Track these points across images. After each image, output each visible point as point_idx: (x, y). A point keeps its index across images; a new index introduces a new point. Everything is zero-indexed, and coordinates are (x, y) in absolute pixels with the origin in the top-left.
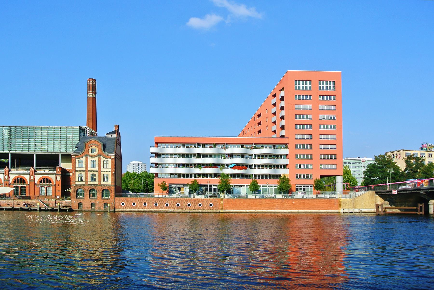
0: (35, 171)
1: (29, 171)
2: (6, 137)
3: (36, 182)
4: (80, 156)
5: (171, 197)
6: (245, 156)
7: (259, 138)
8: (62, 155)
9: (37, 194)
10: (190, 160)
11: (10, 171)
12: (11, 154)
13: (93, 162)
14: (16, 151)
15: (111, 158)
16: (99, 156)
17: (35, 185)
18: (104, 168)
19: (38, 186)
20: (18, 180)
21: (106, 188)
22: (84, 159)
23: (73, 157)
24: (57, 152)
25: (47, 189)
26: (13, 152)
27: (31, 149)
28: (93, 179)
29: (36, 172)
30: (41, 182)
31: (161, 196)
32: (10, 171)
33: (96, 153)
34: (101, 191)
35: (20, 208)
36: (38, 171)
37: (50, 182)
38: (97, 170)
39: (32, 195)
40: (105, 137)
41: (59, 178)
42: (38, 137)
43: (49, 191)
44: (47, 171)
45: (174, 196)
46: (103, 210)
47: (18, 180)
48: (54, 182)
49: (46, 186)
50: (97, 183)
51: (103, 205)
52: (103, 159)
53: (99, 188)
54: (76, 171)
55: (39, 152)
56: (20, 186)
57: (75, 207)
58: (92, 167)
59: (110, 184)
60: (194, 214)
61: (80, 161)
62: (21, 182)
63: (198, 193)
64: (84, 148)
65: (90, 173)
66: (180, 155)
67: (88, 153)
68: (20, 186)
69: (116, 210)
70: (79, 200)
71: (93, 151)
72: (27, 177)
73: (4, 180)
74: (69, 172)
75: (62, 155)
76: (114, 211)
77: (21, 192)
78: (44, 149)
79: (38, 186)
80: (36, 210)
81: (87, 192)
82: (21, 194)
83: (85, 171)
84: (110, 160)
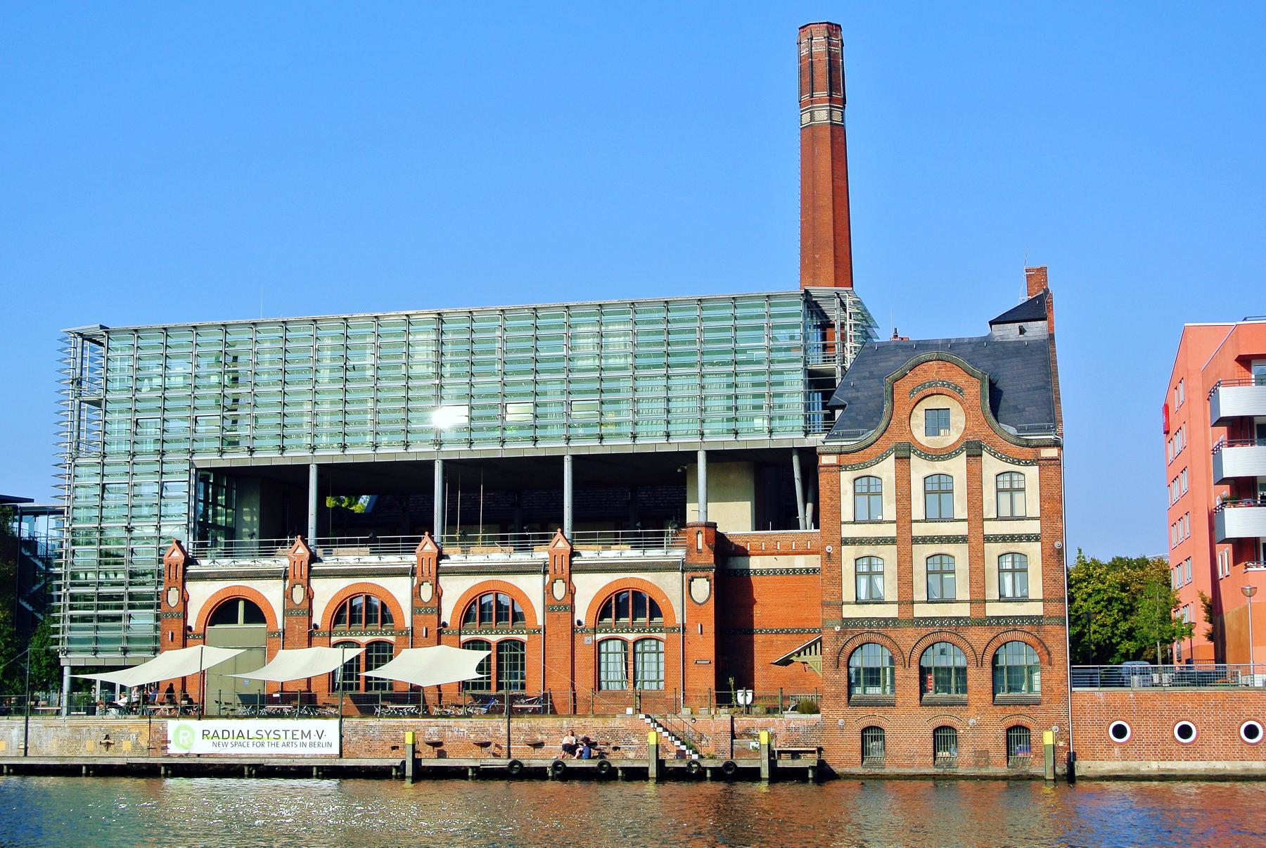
0: (313, 559)
1: (410, 559)
3: (581, 614)
8: (710, 454)
11: (578, 554)
12: (574, 457)
13: (938, 488)
14: (535, 440)
15: (1037, 461)
16: (973, 450)
18: (998, 518)
19: (588, 640)
20: (353, 609)
22: (886, 469)
23: (824, 460)
24: (682, 441)
25: (631, 654)
27: (549, 432)
29: (316, 566)
30: (604, 612)
32: (313, 559)
33: (951, 437)
35: (556, 765)
36: (589, 554)
37: (655, 611)
38: (961, 529)
39: (559, 687)
40: (987, 341)
41: (702, 589)
42: (580, 364)
43: (652, 668)
44: (498, 556)
46: (1002, 770)
47: (353, 609)
48: (677, 609)
49: (631, 637)
52: (991, 466)
54: (845, 542)
55: (591, 447)
56: (494, 638)
57: (844, 757)
59: (1036, 609)
61: (862, 486)
62: (369, 620)
64: (887, 406)
66: (926, 455)
67: (905, 439)
68: (494, 638)
69: (1082, 767)
70: (863, 711)
71: (938, 421)
73: (415, 610)
74: (744, 553)
75: (710, 454)
76: (1070, 777)
77: (499, 676)
78: (612, 429)
79: (588, 640)
80: (637, 774)
82: (500, 686)
83: (892, 541)
84: (1032, 473)
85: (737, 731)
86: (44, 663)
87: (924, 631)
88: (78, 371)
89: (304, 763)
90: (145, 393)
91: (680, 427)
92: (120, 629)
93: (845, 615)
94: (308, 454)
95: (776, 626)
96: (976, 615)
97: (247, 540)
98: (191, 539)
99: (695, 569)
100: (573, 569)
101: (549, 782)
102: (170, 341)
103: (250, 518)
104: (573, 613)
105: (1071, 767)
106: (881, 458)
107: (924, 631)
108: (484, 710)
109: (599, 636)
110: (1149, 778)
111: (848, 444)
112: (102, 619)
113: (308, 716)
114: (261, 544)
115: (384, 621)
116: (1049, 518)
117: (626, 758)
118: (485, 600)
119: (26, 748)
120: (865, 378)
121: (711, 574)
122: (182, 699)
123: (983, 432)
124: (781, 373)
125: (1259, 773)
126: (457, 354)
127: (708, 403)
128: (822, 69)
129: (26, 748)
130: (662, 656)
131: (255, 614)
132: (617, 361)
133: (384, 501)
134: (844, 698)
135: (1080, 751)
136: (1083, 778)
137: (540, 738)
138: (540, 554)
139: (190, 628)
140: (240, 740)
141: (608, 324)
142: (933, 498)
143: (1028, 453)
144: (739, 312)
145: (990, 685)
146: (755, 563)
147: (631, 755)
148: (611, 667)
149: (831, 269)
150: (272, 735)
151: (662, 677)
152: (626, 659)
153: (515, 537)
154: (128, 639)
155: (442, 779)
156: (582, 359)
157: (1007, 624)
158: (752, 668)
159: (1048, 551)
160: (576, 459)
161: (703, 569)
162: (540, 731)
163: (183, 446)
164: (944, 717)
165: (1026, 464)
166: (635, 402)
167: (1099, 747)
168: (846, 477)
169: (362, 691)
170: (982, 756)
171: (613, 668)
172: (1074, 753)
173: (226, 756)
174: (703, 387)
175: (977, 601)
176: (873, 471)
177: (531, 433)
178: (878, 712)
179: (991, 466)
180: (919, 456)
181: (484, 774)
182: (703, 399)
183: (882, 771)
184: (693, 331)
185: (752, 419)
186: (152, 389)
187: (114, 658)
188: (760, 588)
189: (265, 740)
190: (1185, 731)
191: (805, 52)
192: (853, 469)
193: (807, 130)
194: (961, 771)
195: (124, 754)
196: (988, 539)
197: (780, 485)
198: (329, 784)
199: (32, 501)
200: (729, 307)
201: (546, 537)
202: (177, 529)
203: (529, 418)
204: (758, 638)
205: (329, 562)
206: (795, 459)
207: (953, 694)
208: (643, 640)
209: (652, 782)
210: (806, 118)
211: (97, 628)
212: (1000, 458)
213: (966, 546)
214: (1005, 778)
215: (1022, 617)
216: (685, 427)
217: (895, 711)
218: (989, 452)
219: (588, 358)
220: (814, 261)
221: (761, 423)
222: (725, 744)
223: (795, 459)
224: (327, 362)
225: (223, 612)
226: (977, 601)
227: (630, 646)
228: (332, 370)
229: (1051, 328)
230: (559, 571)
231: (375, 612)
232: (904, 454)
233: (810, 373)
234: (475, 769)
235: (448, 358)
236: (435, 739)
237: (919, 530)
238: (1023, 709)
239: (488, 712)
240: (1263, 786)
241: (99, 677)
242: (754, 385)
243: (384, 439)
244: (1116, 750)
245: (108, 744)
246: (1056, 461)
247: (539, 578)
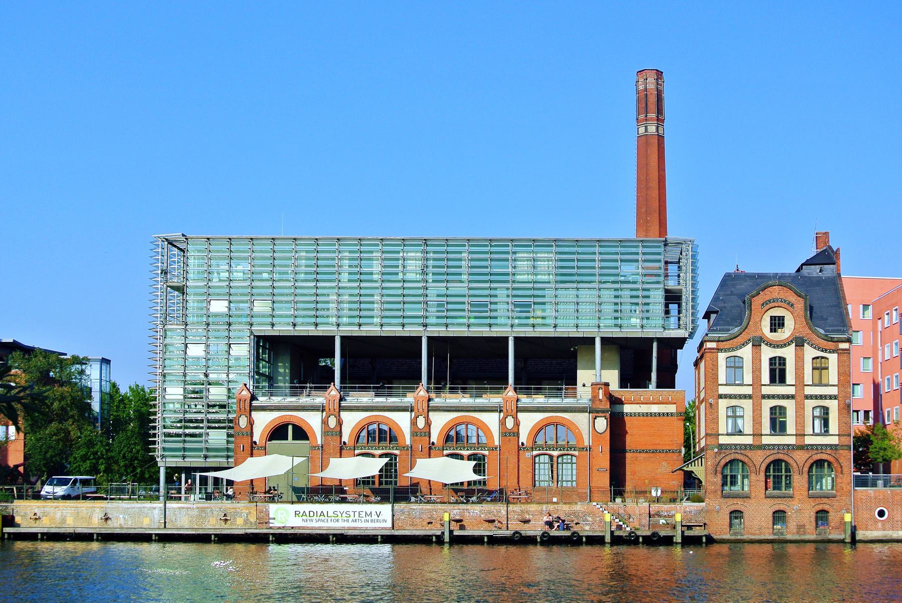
2: (410, 276)
8: (603, 339)
12: (430, 339)
14: (316, 325)
16: (799, 343)
19: (528, 455)
21: (824, 457)
22: (746, 352)
28: (778, 426)
29: (255, 403)
30: (448, 438)
34: (806, 469)
35: (543, 536)
38: (748, 391)
39: (510, 483)
41: (602, 424)
42: (518, 277)
44: (465, 400)
46: (813, 537)
49: (555, 453)
50: (792, 440)
51: (813, 519)
52: (810, 353)
53: (800, 457)
54: (721, 397)
55: (353, 331)
58: (817, 381)
59: (834, 440)
60: (70, 545)
65: (768, 404)
67: (758, 334)
71: (777, 323)
72: (403, 420)
75: (603, 339)
76: (854, 541)
81: (757, 473)
83: (792, 397)
84: (833, 358)
85: (652, 513)
86: (122, 464)
87: (768, 453)
88: (165, 264)
90: (215, 282)
91: (584, 321)
92: (201, 442)
93: (721, 442)
95: (639, 448)
96: (800, 443)
97: (281, 384)
98: (252, 383)
99: (598, 412)
103: (283, 369)
104: (341, 437)
105: (853, 535)
106: (744, 345)
107: (768, 453)
108: (489, 499)
109: (535, 453)
111: (724, 335)
112: (186, 435)
114: (291, 387)
115: (391, 441)
116: (843, 385)
117: (586, 529)
118: (371, 428)
119: (165, 523)
120: (728, 295)
121: (608, 415)
123: (805, 332)
125: (351, 533)
127: (603, 307)
128: (653, 99)
129: (165, 523)
130: (574, 465)
131: (301, 434)
132: (526, 277)
133: (380, 363)
134: (719, 493)
136: (861, 541)
137: (527, 517)
138: (409, 399)
139: (255, 443)
140: (322, 518)
141: (407, 252)
143: (831, 345)
144: (363, 248)
145: (806, 486)
146: (627, 409)
147: (587, 528)
148: (542, 472)
149: (657, 227)
150: (344, 515)
151: (574, 478)
152: (552, 466)
153: (374, 388)
154: (208, 449)
155: (463, 544)
156: (520, 274)
157: (817, 449)
159: (842, 406)
161: (603, 412)
163: (244, 320)
164: (780, 505)
165: (830, 352)
166: (557, 304)
167: (870, 523)
168: (722, 356)
169: (377, 485)
172: (855, 527)
173: (312, 528)
174: (556, 296)
175: (800, 435)
176: (738, 353)
177: (270, 320)
178: (739, 501)
179: (810, 353)
180: (767, 344)
181: (494, 541)
182: (600, 304)
183: (742, 537)
184: (334, 259)
185: (630, 317)
186: (220, 280)
187: (222, 461)
188: (629, 423)
189: (339, 517)
192: (725, 351)
193: (643, 138)
194: (789, 537)
195: (238, 526)
196: (807, 397)
197: (643, 361)
198: (386, 549)
199: (66, 354)
200: (356, 245)
201: (413, 388)
203: (268, 310)
204: (629, 456)
205: (262, 400)
206: (655, 345)
207: (784, 491)
208: (562, 455)
209: (446, 547)
210: (642, 130)
211: (185, 441)
212: (815, 348)
213: (793, 401)
215: (826, 445)
216: (588, 321)
217: (750, 501)
218: (808, 344)
219: (524, 274)
220: (647, 221)
221: (635, 321)
222: (645, 521)
223: (655, 345)
225: (278, 433)
226: (800, 435)
227: (555, 459)
228: (350, 274)
229: (838, 269)
230: (421, 410)
231: (383, 436)
232: (758, 342)
233: (667, 291)
234: (489, 537)
235: (430, 269)
236: (458, 518)
238: (825, 500)
239: (491, 501)
240: (896, 546)
241: (211, 474)
243: (299, 320)
244: (880, 524)
245: (226, 520)
246: (847, 351)
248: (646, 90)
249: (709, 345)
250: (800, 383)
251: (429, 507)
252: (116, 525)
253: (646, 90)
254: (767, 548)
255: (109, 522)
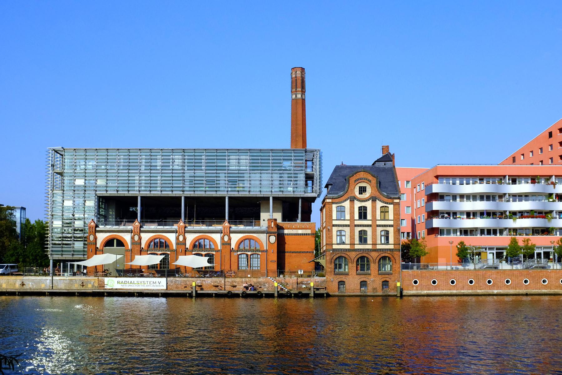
2: (176, 167)
4: (337, 200)
5: (467, 268)
6: (446, 198)
7: (514, 169)
9: (234, 267)
10: (497, 205)
17: (231, 251)
19: (236, 254)
21: (387, 255)
22: (347, 204)
24: (264, 194)
26: (188, 194)
28: (363, 239)
29: (97, 229)
31: (449, 268)
35: (243, 293)
36: (146, 227)
38: (348, 223)
41: (273, 239)
42: (231, 168)
44: (204, 227)
45: (471, 267)
48: (265, 245)
49: (249, 253)
50: (370, 247)
52: (379, 204)
55: (147, 194)
59: (392, 247)
63: (511, 262)
65: (358, 229)
69: (405, 292)
71: (362, 190)
75: (274, 198)
76: (402, 296)
83: (348, 226)
84: (391, 207)
86: (31, 258)
87: (358, 253)
89: (157, 292)
94: (138, 193)
99: (271, 233)
100: (141, 232)
101: (293, 299)
102: (87, 154)
105: (401, 293)
107: (358, 253)
109: (239, 253)
110: (423, 296)
113: (133, 277)
115: (166, 247)
117: (265, 290)
118: (156, 241)
121: (276, 235)
122: (105, 272)
123: (377, 194)
124: (219, 173)
126: (124, 163)
128: (299, 82)
131: (120, 243)
133: (160, 209)
135: (404, 288)
136: (405, 296)
137: (235, 284)
138: (175, 227)
142: (383, 214)
143: (390, 201)
148: (242, 262)
154: (74, 251)
158: (285, 263)
160: (142, 198)
161: (274, 233)
162: (235, 282)
163: (92, 189)
168: (334, 206)
170: (375, 289)
171: (243, 262)
176: (343, 204)
179: (379, 204)
180: (380, 201)
181: (218, 296)
182: (272, 181)
185: (288, 187)
190: (434, 282)
191: (294, 76)
192: (336, 204)
194: (369, 294)
195: (89, 288)
197: (294, 208)
198: (163, 300)
202: (91, 216)
205: (101, 227)
206: (300, 200)
210: (294, 96)
211: (62, 247)
213: (371, 228)
214: (165, 295)
215: (387, 249)
217: (349, 277)
221: (290, 189)
223: (300, 200)
224: (144, 163)
225: (109, 243)
228: (145, 166)
229: (394, 164)
237: (379, 223)
238: (387, 276)
242: (288, 177)
244: (415, 288)
246: (398, 204)
247: (175, 234)
248: (296, 77)
249: (328, 201)
250: (374, 219)
251: (185, 279)
252: (28, 288)
253: (296, 77)
254: (358, 299)
255: (24, 286)
